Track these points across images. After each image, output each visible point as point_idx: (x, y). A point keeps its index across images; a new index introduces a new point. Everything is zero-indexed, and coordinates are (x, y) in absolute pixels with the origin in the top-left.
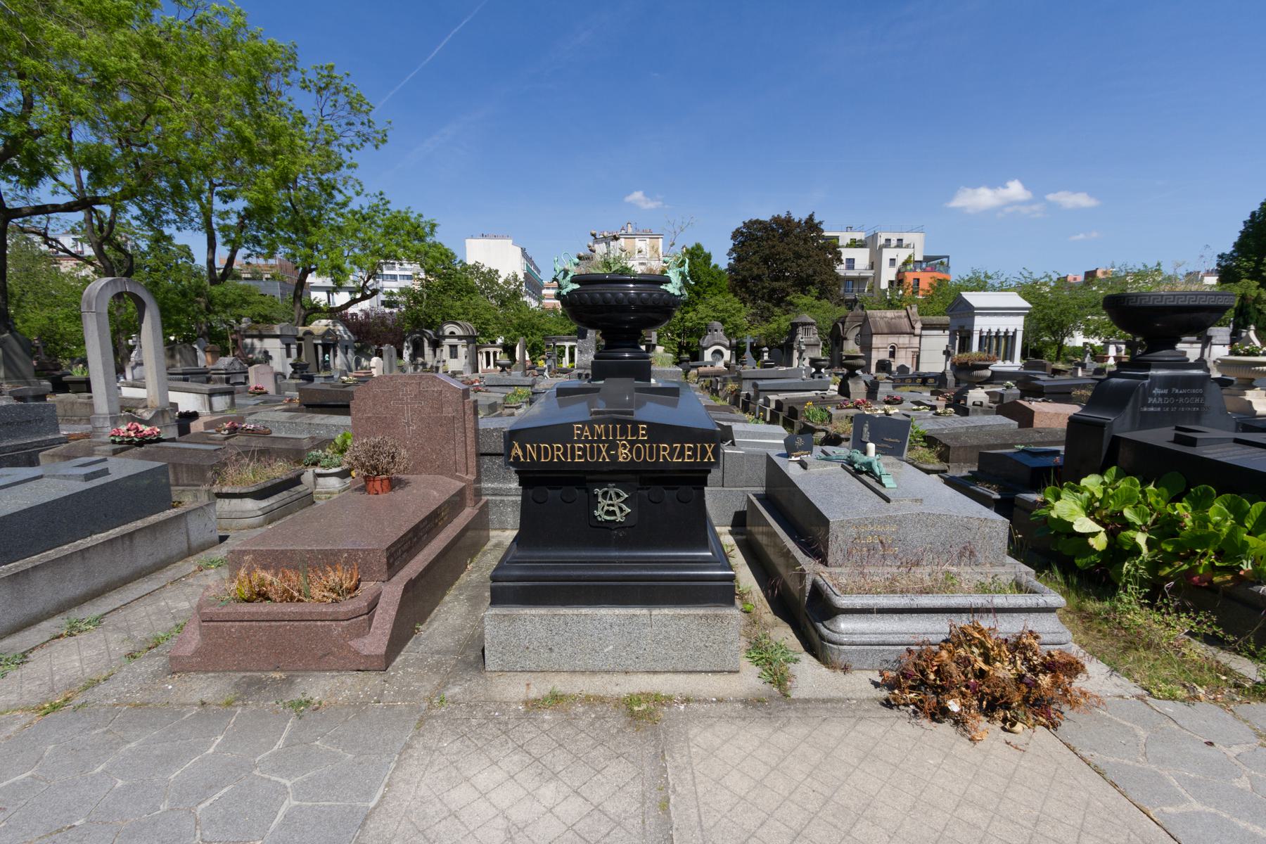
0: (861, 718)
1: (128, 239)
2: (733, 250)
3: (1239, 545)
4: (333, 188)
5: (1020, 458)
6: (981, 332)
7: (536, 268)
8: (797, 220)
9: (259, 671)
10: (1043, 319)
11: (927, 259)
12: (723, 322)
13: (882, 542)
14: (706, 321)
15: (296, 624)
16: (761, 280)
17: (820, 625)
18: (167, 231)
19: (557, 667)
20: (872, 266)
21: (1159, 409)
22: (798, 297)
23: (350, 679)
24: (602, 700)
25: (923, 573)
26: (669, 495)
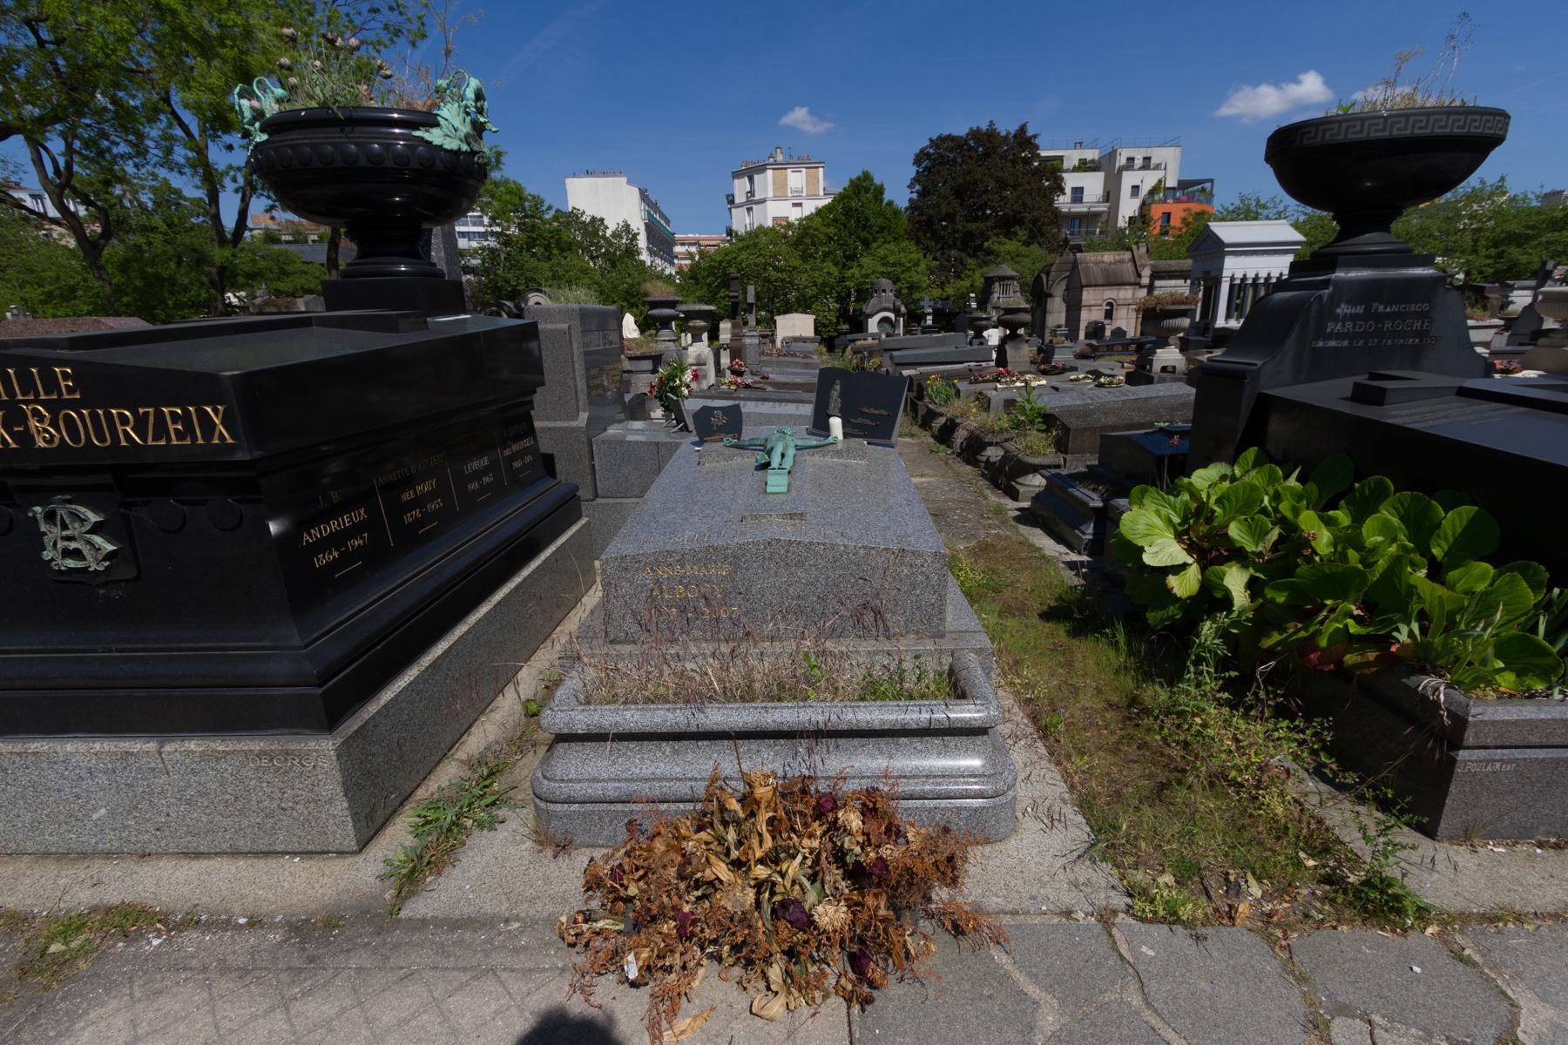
2: (916, 180)
3: (1403, 592)
6: (1233, 278)
7: (663, 216)
8: (1003, 134)
11: (1183, 185)
19: (13, 846)
21: (1346, 343)
22: (999, 243)
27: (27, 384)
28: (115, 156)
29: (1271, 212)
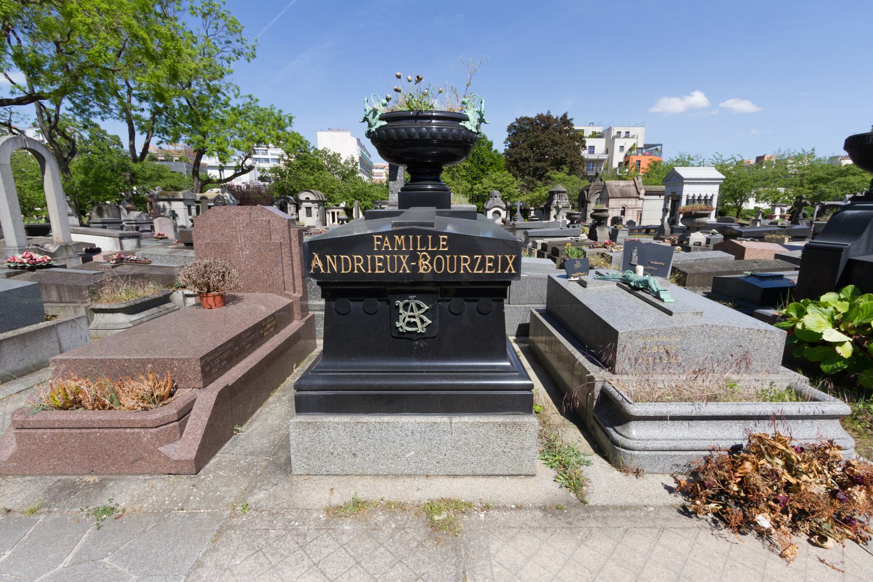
0: (663, 529)
1: (75, 131)
2: (508, 139)
4: (218, 91)
5: (753, 281)
6: (688, 196)
7: (368, 153)
8: (555, 117)
9: (74, 474)
10: (728, 190)
11: (647, 146)
12: (501, 191)
13: (667, 352)
14: (489, 190)
15: (106, 431)
16: (528, 161)
17: (611, 430)
18: (94, 120)
19: (361, 471)
20: (607, 152)
22: (555, 173)
23: (159, 483)
24: (402, 507)
25: (709, 383)
26: (469, 306)
27: (424, 243)
28: (90, 113)
29: (695, 163)
